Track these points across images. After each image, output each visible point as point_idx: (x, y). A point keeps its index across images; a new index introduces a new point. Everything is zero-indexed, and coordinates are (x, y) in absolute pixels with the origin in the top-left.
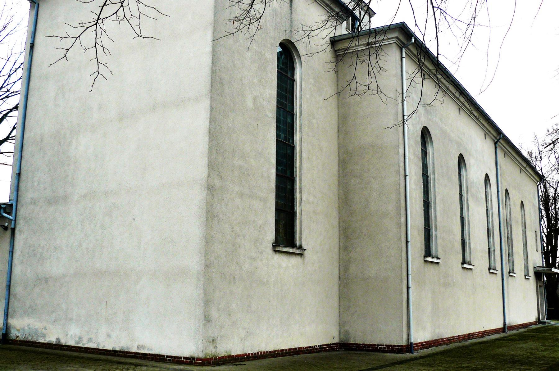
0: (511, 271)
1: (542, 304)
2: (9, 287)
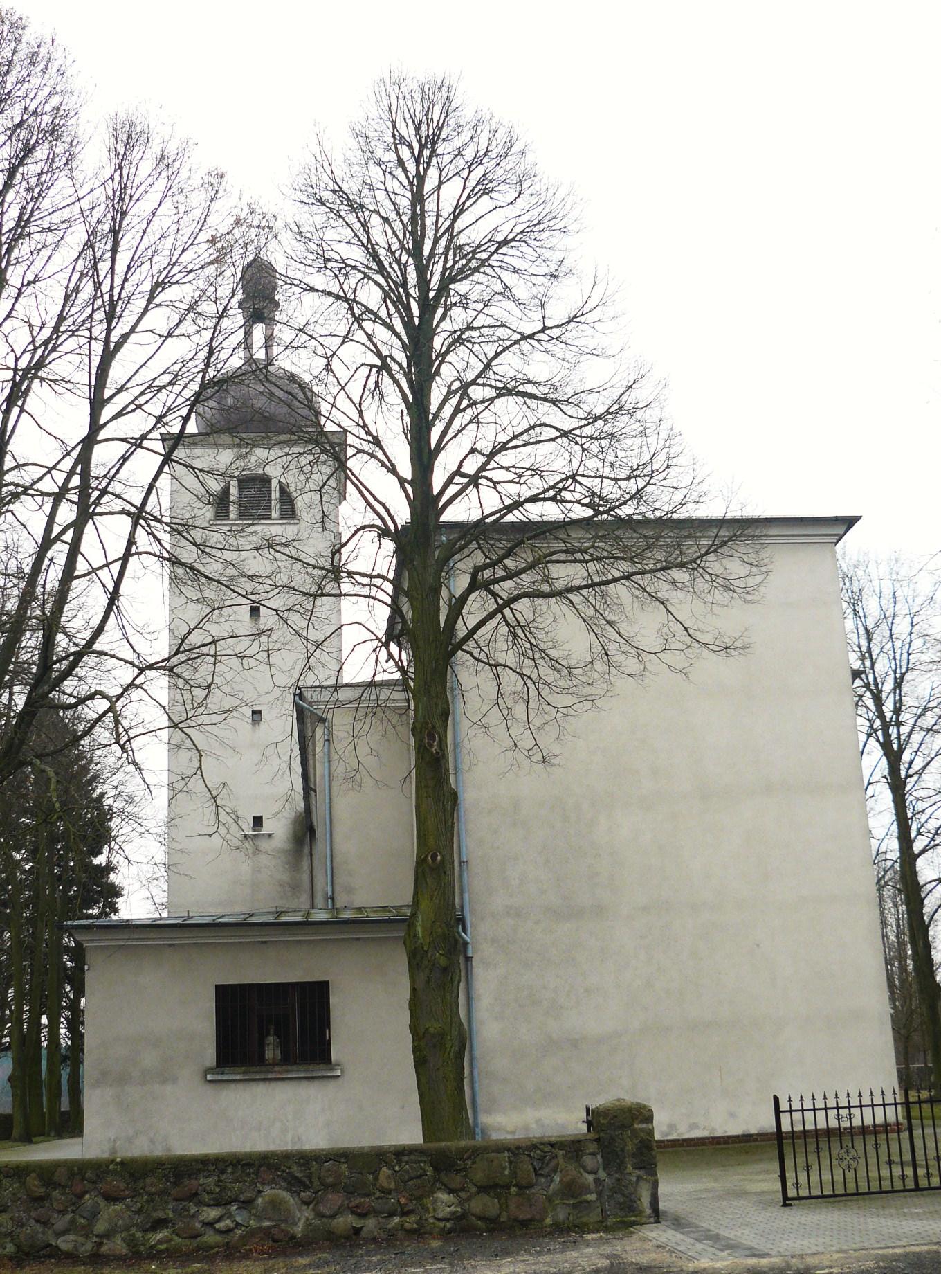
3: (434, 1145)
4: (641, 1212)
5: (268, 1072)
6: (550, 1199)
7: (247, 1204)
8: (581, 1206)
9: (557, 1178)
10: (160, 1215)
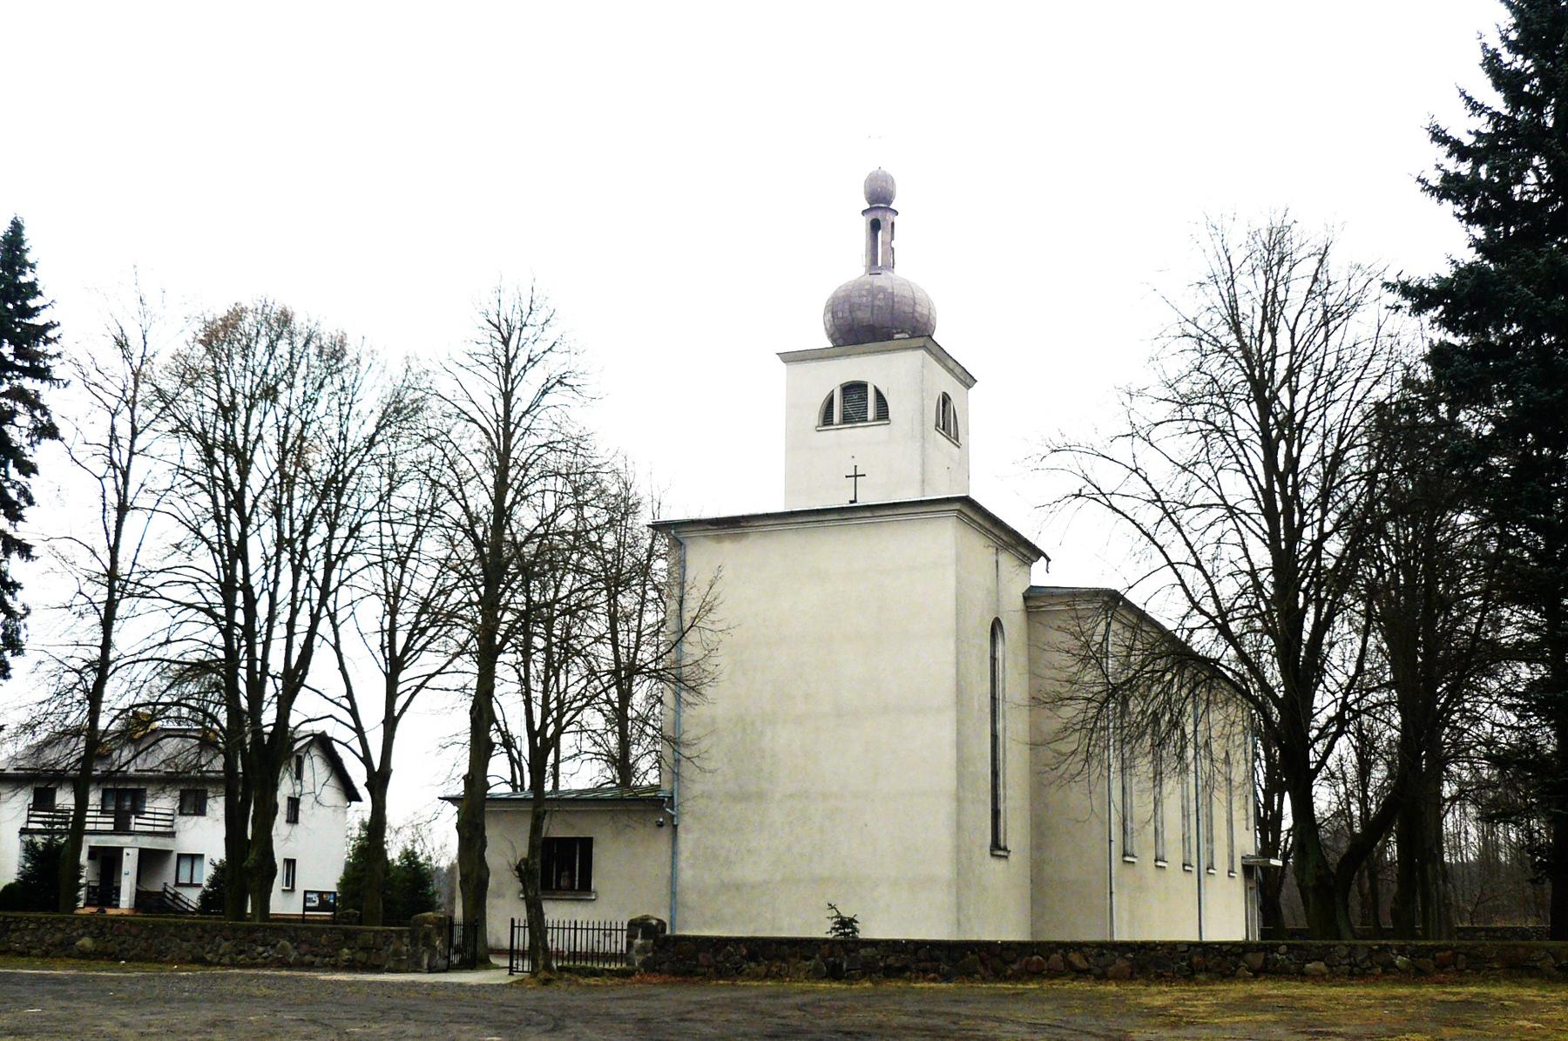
0: (1211, 866)
1: (1253, 920)
2: (673, 894)
3: (1264, 942)
4: (421, 967)
5: (554, 894)
6: (388, 956)
7: (274, 946)
8: (400, 961)
9: (392, 947)
10: (242, 948)
